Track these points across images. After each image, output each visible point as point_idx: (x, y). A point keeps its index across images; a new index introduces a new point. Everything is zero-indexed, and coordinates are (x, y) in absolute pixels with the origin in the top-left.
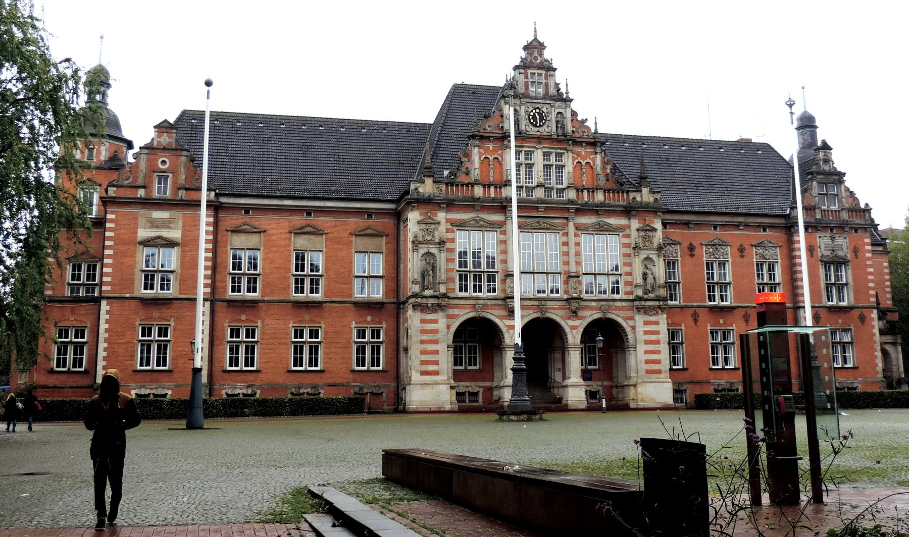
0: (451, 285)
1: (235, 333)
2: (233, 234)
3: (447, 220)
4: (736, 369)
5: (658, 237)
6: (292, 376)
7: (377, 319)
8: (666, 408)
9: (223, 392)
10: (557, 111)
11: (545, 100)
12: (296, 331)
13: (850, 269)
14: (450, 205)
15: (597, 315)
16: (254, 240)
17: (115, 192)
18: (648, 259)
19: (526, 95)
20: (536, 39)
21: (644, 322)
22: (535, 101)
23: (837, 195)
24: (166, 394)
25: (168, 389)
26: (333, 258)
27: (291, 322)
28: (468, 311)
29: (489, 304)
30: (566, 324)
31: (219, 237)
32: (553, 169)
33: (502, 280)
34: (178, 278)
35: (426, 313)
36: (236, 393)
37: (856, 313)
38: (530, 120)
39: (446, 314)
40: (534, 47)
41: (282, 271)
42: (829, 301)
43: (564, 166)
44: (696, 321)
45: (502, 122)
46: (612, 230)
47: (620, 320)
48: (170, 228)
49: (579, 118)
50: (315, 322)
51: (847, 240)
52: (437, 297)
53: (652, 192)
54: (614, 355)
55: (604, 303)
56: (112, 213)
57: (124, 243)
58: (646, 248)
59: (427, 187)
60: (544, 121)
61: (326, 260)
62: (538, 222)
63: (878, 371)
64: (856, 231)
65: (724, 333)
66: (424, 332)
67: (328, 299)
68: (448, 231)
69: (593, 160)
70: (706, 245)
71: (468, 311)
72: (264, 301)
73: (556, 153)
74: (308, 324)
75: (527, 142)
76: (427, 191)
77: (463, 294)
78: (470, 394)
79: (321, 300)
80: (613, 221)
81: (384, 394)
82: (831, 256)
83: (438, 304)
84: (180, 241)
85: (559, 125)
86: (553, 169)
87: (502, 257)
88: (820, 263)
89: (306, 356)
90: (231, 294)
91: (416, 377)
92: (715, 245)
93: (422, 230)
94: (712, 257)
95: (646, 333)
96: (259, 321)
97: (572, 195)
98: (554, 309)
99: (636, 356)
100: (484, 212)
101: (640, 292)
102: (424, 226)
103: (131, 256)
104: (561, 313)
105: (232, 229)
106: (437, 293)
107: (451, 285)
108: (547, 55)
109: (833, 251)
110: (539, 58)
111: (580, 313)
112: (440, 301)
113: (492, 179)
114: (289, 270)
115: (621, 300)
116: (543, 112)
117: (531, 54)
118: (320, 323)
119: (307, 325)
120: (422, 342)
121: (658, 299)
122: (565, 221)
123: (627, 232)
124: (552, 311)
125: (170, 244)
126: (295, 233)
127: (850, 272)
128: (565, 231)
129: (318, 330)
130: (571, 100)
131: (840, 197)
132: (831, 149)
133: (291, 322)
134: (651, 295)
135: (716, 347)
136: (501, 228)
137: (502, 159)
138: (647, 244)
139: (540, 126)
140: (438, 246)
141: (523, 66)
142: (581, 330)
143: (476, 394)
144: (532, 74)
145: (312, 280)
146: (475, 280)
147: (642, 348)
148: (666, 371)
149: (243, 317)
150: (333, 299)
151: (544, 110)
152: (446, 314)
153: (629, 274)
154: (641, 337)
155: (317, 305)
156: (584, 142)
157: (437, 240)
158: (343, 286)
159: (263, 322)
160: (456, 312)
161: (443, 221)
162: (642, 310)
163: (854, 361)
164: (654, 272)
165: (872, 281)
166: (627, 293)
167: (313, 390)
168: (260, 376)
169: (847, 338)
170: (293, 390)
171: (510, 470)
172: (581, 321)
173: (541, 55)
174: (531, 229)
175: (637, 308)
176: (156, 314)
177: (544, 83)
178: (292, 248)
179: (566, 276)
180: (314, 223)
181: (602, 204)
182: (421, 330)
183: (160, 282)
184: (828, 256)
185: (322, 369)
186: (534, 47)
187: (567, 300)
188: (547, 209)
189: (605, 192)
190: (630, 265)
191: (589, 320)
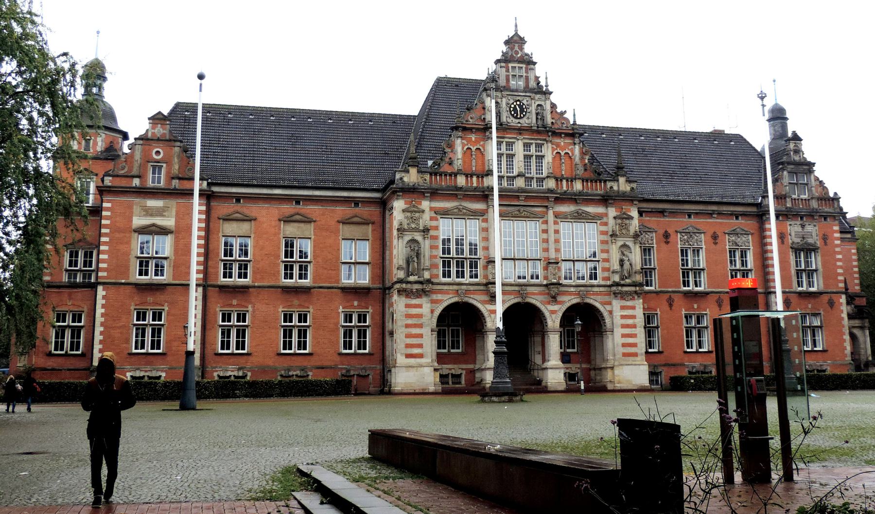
0: (435, 271)
1: (226, 317)
2: (225, 222)
3: (431, 209)
4: (709, 352)
5: (635, 225)
7: (363, 304)
8: (642, 390)
10: (537, 103)
11: (526, 92)
12: (285, 315)
13: (820, 256)
14: (434, 194)
15: (576, 300)
16: (245, 227)
18: (625, 246)
19: (507, 88)
20: (516, 34)
22: (516, 94)
23: (807, 184)
24: (160, 376)
25: (162, 371)
26: (321, 245)
27: (281, 307)
32: (534, 159)
34: (172, 265)
37: (825, 298)
38: (511, 112)
39: (430, 299)
40: (515, 42)
42: (799, 286)
43: (543, 156)
44: (671, 305)
49: (559, 110)
50: (304, 307)
51: (817, 228)
54: (592, 338)
55: (582, 288)
56: (108, 201)
58: (623, 235)
59: (412, 177)
60: (524, 113)
61: (314, 246)
62: (519, 211)
63: (846, 354)
65: (698, 317)
67: (316, 285)
68: (432, 219)
69: (572, 150)
70: (680, 232)
71: (451, 296)
72: (254, 287)
73: (536, 144)
76: (412, 180)
77: (447, 280)
78: (453, 376)
79: (309, 285)
80: (591, 209)
81: (370, 376)
82: (801, 243)
83: (422, 289)
84: (173, 228)
85: (539, 117)
86: (534, 159)
87: (483, 244)
88: (791, 250)
91: (401, 360)
92: (689, 233)
94: (687, 244)
95: (623, 317)
97: (551, 184)
99: (613, 339)
101: (617, 278)
102: (409, 214)
104: (541, 298)
106: (421, 279)
107: (435, 271)
108: (527, 49)
109: (803, 238)
110: (520, 52)
116: (523, 104)
117: (512, 49)
118: (308, 308)
121: (634, 285)
122: (544, 210)
123: (605, 220)
124: (533, 296)
125: (163, 231)
126: (284, 221)
127: (819, 258)
129: (307, 314)
130: (551, 93)
131: (810, 186)
132: (800, 140)
133: (281, 307)
134: (628, 281)
135: (691, 330)
138: (624, 232)
140: (422, 234)
141: (505, 60)
142: (560, 314)
144: (514, 68)
146: (457, 266)
147: (618, 331)
148: (642, 354)
149: (235, 302)
151: (525, 102)
153: (607, 260)
154: (618, 321)
156: (563, 133)
157: (421, 228)
158: (330, 272)
159: (253, 307)
160: (439, 297)
161: (427, 210)
163: (823, 344)
164: (630, 259)
165: (841, 267)
166: (604, 279)
169: (817, 322)
171: (492, 449)
173: (521, 49)
174: (512, 217)
175: (614, 294)
176: (150, 299)
177: (524, 76)
180: (302, 212)
181: (580, 193)
182: (406, 315)
184: (798, 243)
185: (311, 352)
186: (515, 42)
187: (546, 285)
190: (607, 251)
191: (568, 305)
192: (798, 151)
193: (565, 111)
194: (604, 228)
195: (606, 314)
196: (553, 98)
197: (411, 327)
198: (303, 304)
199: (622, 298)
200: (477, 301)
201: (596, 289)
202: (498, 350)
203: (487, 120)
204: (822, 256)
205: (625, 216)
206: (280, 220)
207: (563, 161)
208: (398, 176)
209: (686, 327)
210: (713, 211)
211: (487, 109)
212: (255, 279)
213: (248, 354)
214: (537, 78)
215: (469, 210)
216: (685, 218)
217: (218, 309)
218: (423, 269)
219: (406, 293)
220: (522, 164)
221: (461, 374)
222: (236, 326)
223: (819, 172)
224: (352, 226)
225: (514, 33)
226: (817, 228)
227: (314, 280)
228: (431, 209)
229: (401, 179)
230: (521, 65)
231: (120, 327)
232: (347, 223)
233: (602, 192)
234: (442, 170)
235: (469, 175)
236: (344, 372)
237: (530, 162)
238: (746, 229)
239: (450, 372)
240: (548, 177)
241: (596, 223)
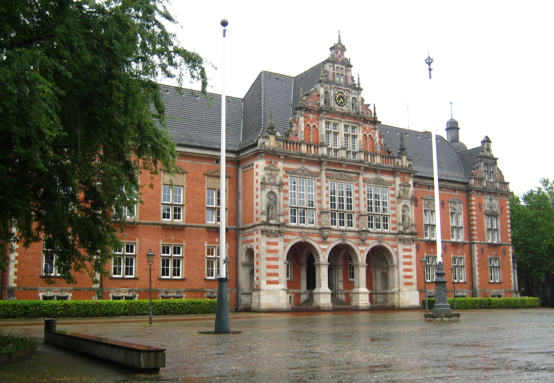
3: (284, 168)
4: (464, 283)
6: (162, 283)
9: (41, 295)
10: (353, 96)
11: (346, 87)
12: (164, 248)
14: (287, 158)
15: (376, 244)
19: (334, 82)
22: (340, 87)
23: (493, 172)
24: (67, 296)
25: (69, 292)
27: (161, 241)
29: (310, 232)
35: (270, 237)
37: (502, 248)
39: (283, 238)
41: (155, 200)
45: (319, 100)
47: (389, 247)
49: (365, 103)
51: (498, 201)
52: (279, 226)
53: (408, 159)
54: (374, 272)
55: (380, 235)
58: (405, 198)
59: (271, 143)
61: (187, 193)
62: (341, 175)
64: (502, 195)
66: (269, 251)
67: (188, 224)
69: (373, 133)
70: (424, 199)
71: (297, 237)
72: (141, 223)
74: (173, 242)
75: (335, 116)
76: (271, 145)
77: (293, 224)
82: (490, 211)
83: (279, 231)
85: (354, 107)
87: (318, 198)
89: (171, 268)
91: (263, 284)
92: (429, 199)
96: (137, 239)
98: (350, 238)
99: (399, 272)
100: (308, 164)
101: (401, 229)
102: (269, 172)
104: (354, 241)
106: (278, 223)
107: (286, 217)
108: (347, 55)
109: (491, 208)
111: (367, 242)
112: (281, 228)
113: (312, 140)
114: (160, 199)
115: (390, 234)
116: (344, 96)
118: (182, 242)
119: (173, 244)
120: (268, 259)
121: (412, 234)
122: (356, 175)
123: (393, 186)
124: (350, 239)
126: (164, 171)
128: (357, 182)
129: (180, 247)
130: (362, 90)
131: (494, 174)
132: (490, 142)
133: (161, 241)
134: (408, 231)
136: (317, 177)
139: (342, 106)
140: (278, 187)
142: (366, 253)
144: (338, 68)
147: (402, 267)
150: (191, 224)
151: (345, 94)
152: (283, 238)
153: (394, 215)
154: (402, 260)
155: (179, 229)
156: (369, 120)
157: (278, 183)
158: (198, 214)
159: (140, 240)
160: (288, 237)
161: (282, 169)
163: (500, 279)
166: (394, 229)
167: (178, 294)
168: (138, 282)
171: (68, 334)
173: (342, 54)
175: (400, 240)
179: (357, 215)
181: (379, 166)
185: (184, 277)
186: (338, 48)
187: (358, 232)
188: (348, 166)
191: (371, 247)
192: (489, 150)
193: (369, 105)
194: (392, 192)
195: (393, 254)
196: (363, 94)
197: (271, 260)
198: (177, 239)
199: (404, 243)
200: (314, 241)
201: (388, 236)
202: (438, 280)
203: (321, 105)
204: (501, 220)
205: (406, 184)
207: (368, 141)
208: (261, 141)
210: (443, 185)
211: (321, 96)
212: (142, 217)
213: (135, 279)
214: (352, 78)
215: (309, 172)
216: (426, 189)
218: (279, 215)
220: (343, 140)
223: (500, 165)
224: (213, 178)
226: (498, 201)
227: (187, 219)
228: (284, 168)
229: (263, 143)
230: (343, 67)
231: (33, 253)
232: (212, 176)
233: (392, 166)
234: (290, 139)
235: (309, 145)
236: (209, 294)
238: (460, 199)
240: (360, 151)
241: (388, 188)
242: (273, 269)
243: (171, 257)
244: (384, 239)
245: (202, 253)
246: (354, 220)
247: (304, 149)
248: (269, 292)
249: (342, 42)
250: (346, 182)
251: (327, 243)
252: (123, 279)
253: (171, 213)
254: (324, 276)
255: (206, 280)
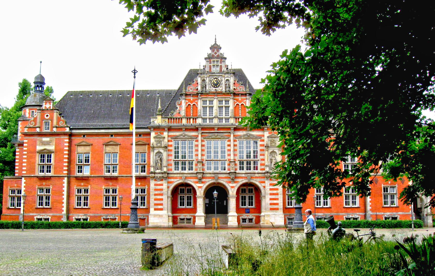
0: (170, 167)
1: (79, 191)
2: (78, 147)
3: (169, 136)
7: (143, 184)
8: (168, 228)
10: (226, 79)
14: (170, 129)
15: (245, 181)
16: (88, 149)
17: (27, 130)
18: (273, 152)
20: (215, 44)
21: (270, 184)
26: (123, 156)
27: (104, 186)
28: (178, 179)
30: (229, 186)
31: (72, 148)
32: (224, 109)
33: (196, 164)
36: (79, 218)
38: (212, 84)
46: (254, 137)
47: (257, 183)
48: (50, 145)
50: (114, 186)
52: (162, 173)
55: (249, 175)
56: (26, 139)
57: (31, 153)
59: (158, 121)
66: (156, 190)
67: (120, 175)
68: (169, 141)
72: (91, 177)
73: (225, 100)
78: (187, 219)
84: (54, 151)
86: (224, 109)
89: (111, 201)
90: (78, 173)
93: (155, 141)
98: (222, 178)
101: (267, 169)
103: (34, 158)
105: (77, 144)
106: (162, 171)
107: (170, 167)
115: (258, 173)
116: (219, 80)
117: (213, 51)
118: (116, 186)
120: (155, 195)
123: (263, 138)
124: (222, 179)
126: (106, 145)
133: (104, 186)
135: (393, 195)
137: (197, 105)
138: (273, 144)
141: (209, 58)
142: (236, 188)
143: (190, 219)
145: (47, 167)
146: (182, 164)
147: (268, 197)
148: (281, 209)
149: (82, 184)
150: (122, 175)
151: (219, 79)
156: (240, 94)
158: (127, 169)
159: (91, 186)
160: (172, 180)
161: (166, 137)
162: (269, 178)
164: (276, 158)
166: (261, 169)
170: (104, 217)
172: (236, 184)
174: (212, 139)
176: (44, 183)
178: (104, 152)
180: (114, 140)
182: (155, 189)
183: (141, 169)
185: (330, 206)
187: (229, 173)
188: (219, 129)
189: (187, 119)
190: (264, 155)
195: (262, 188)
201: (256, 175)
206: (103, 145)
209: (384, 194)
213: (51, 208)
217: (75, 188)
219: (155, 179)
221: (191, 218)
222: (112, 195)
225: (214, 43)
231: (32, 196)
234: (175, 117)
237: (222, 110)
239: (185, 217)
242: (159, 201)
243: (350, 194)
244: (253, 178)
245: (129, 192)
246: (194, 166)
247: (184, 121)
248: (155, 216)
249: (217, 43)
250: (219, 140)
251: (202, 182)
252: (322, 208)
253: (45, 169)
254: (200, 204)
255: (383, 207)
